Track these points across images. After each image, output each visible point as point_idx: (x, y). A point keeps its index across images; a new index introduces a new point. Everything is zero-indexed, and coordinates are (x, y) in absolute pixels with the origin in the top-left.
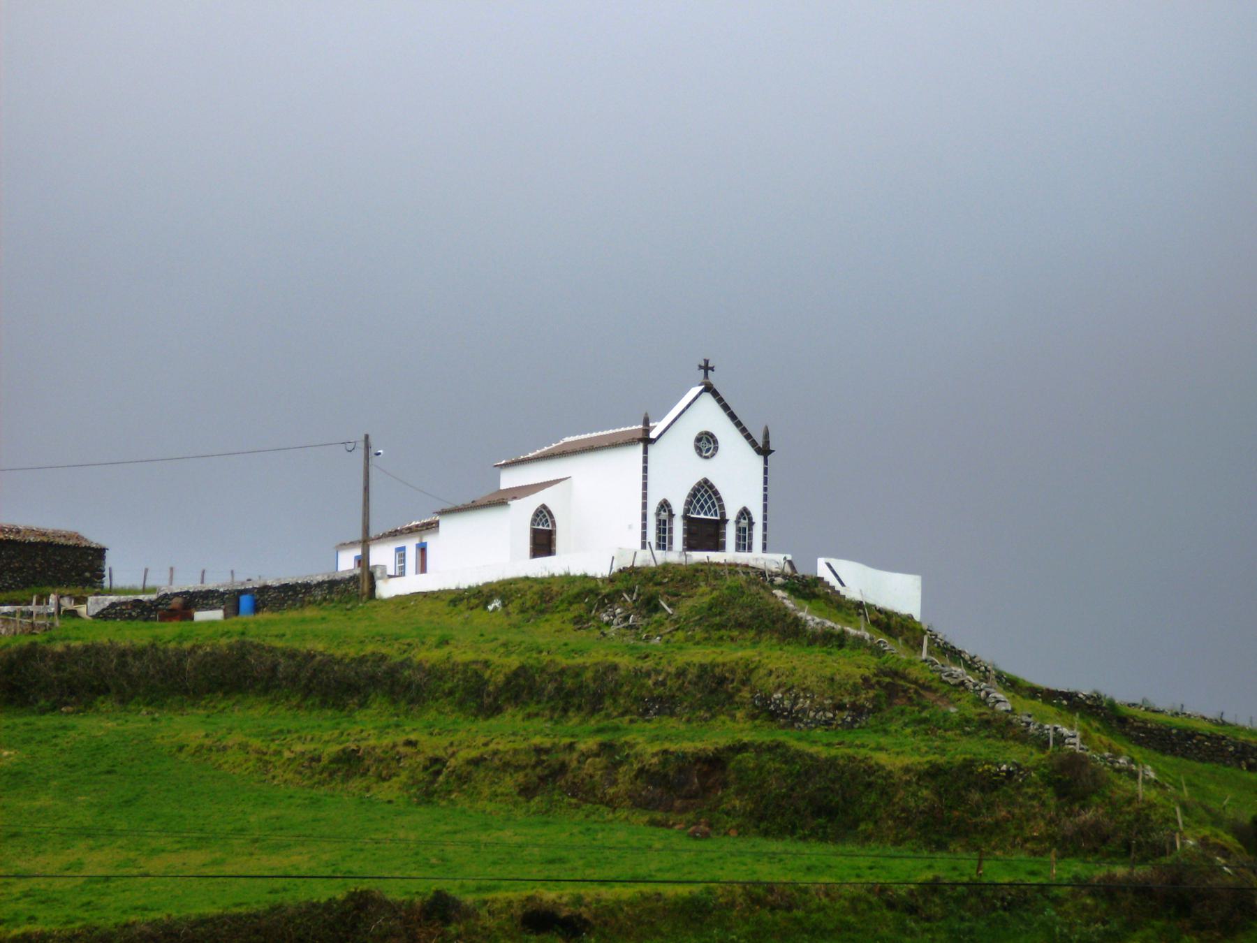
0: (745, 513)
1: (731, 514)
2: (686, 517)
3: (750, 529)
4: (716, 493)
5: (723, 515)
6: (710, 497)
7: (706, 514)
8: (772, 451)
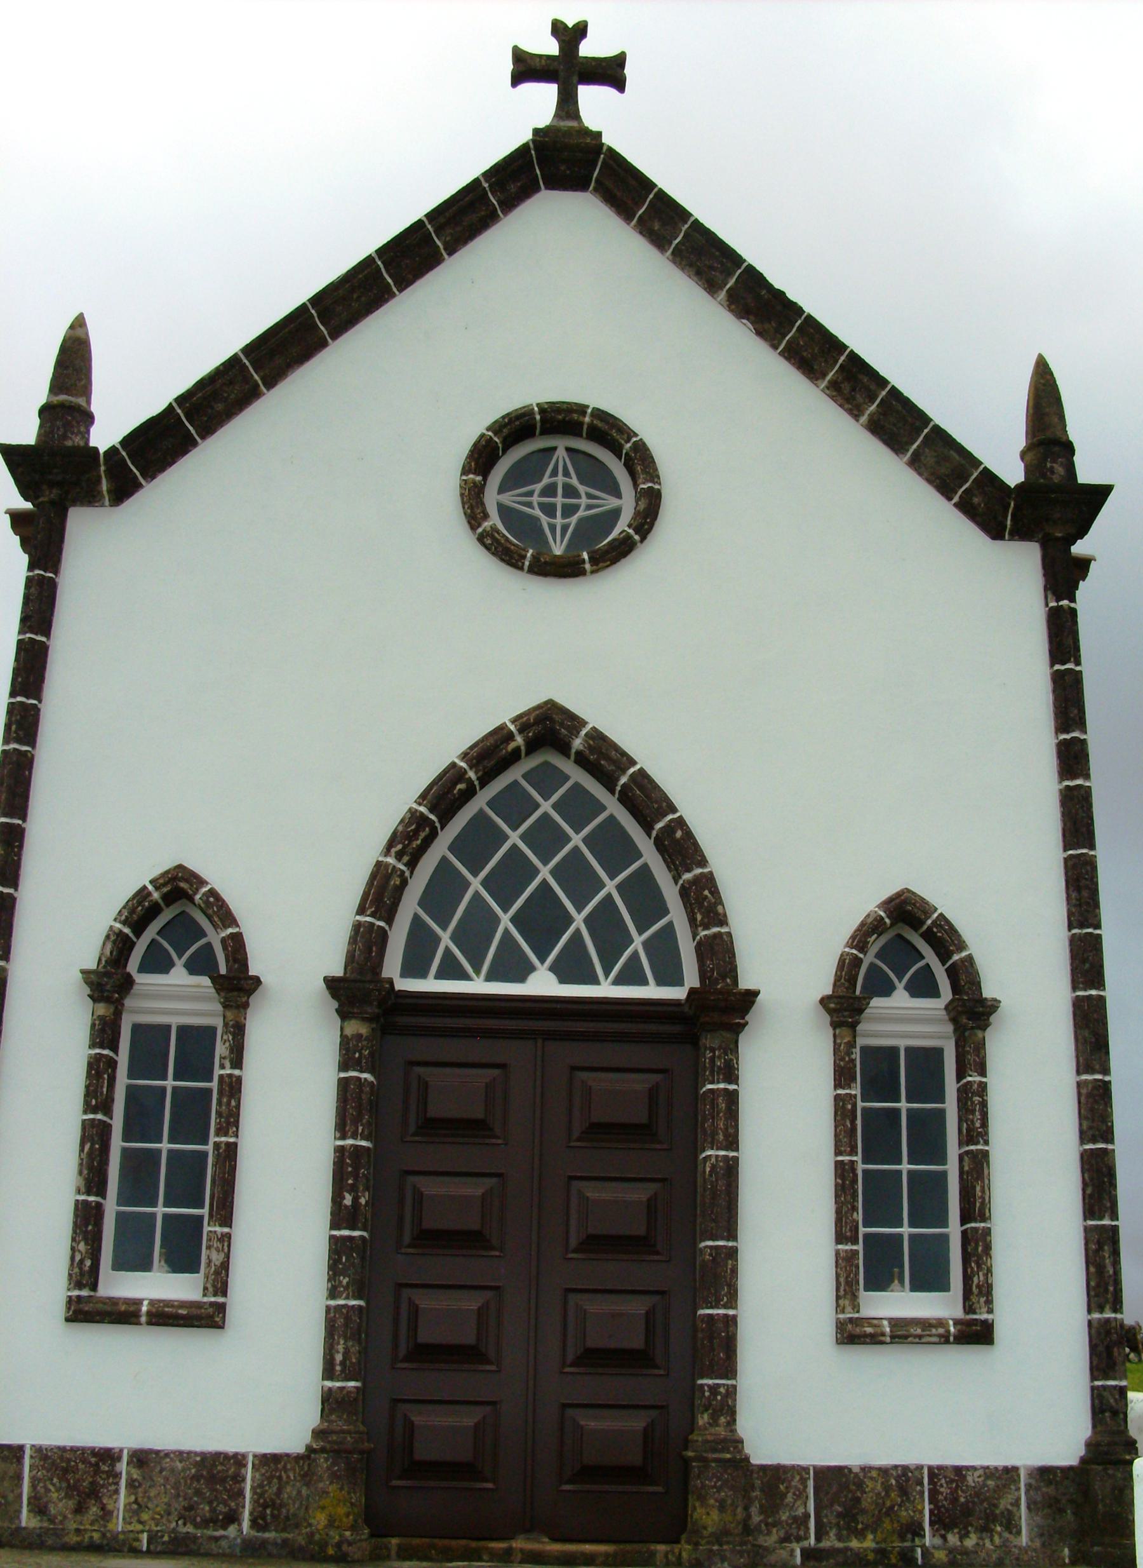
0: (907, 939)
1: (788, 954)
2: (356, 991)
3: (972, 1058)
4: (646, 800)
5: (718, 955)
6: (614, 848)
7: (572, 967)
8: (1099, 494)
